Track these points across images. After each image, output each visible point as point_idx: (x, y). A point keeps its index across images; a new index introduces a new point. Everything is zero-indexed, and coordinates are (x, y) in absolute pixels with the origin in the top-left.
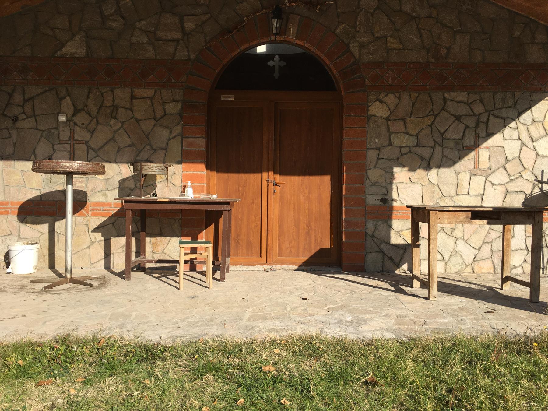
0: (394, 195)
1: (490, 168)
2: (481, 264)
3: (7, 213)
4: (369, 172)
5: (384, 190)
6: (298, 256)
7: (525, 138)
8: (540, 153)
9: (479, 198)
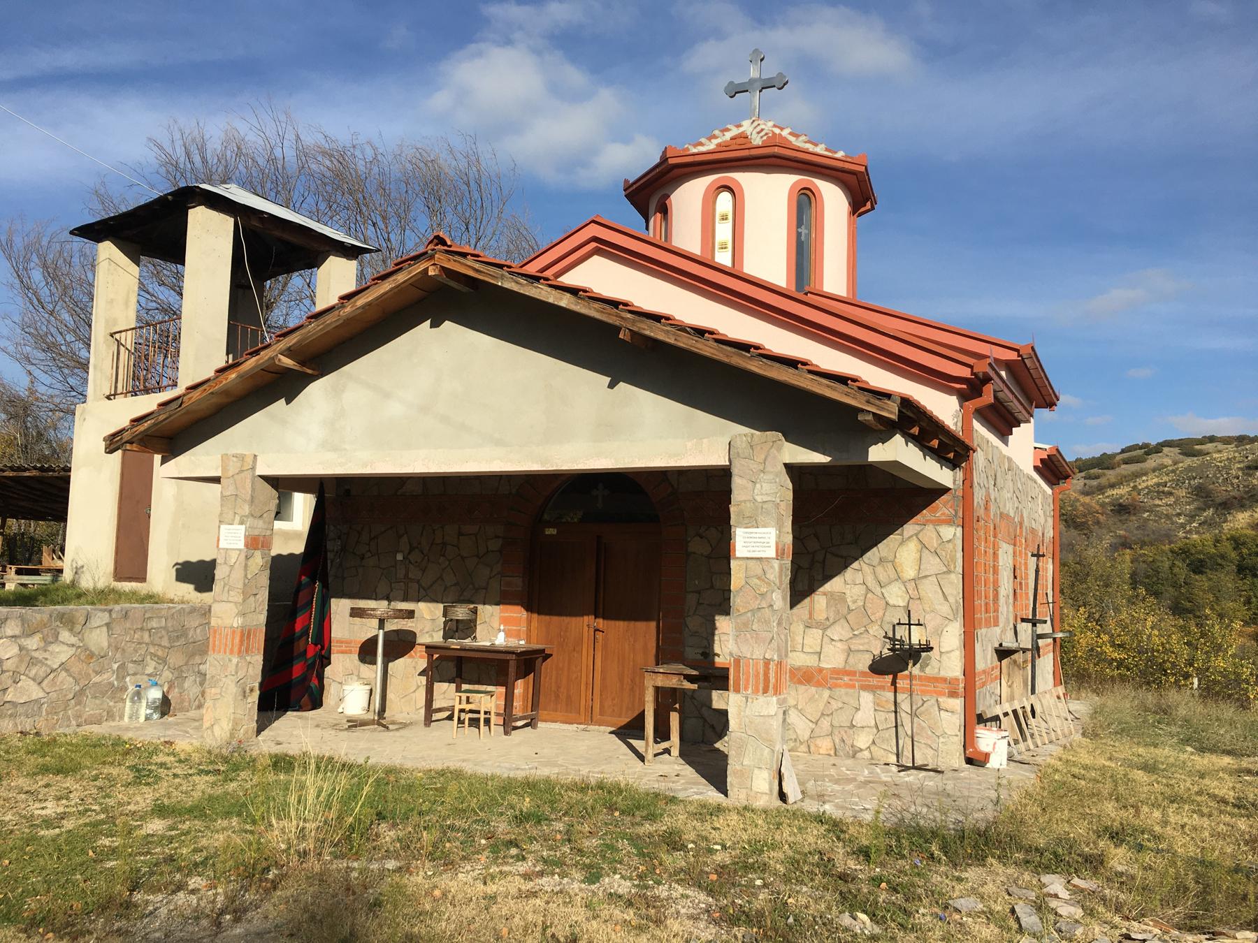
0: (717, 649)
1: (827, 619)
2: (819, 742)
3: (350, 652)
4: (688, 620)
5: (705, 643)
6: (620, 716)
7: (870, 581)
8: (891, 602)
9: (816, 657)
